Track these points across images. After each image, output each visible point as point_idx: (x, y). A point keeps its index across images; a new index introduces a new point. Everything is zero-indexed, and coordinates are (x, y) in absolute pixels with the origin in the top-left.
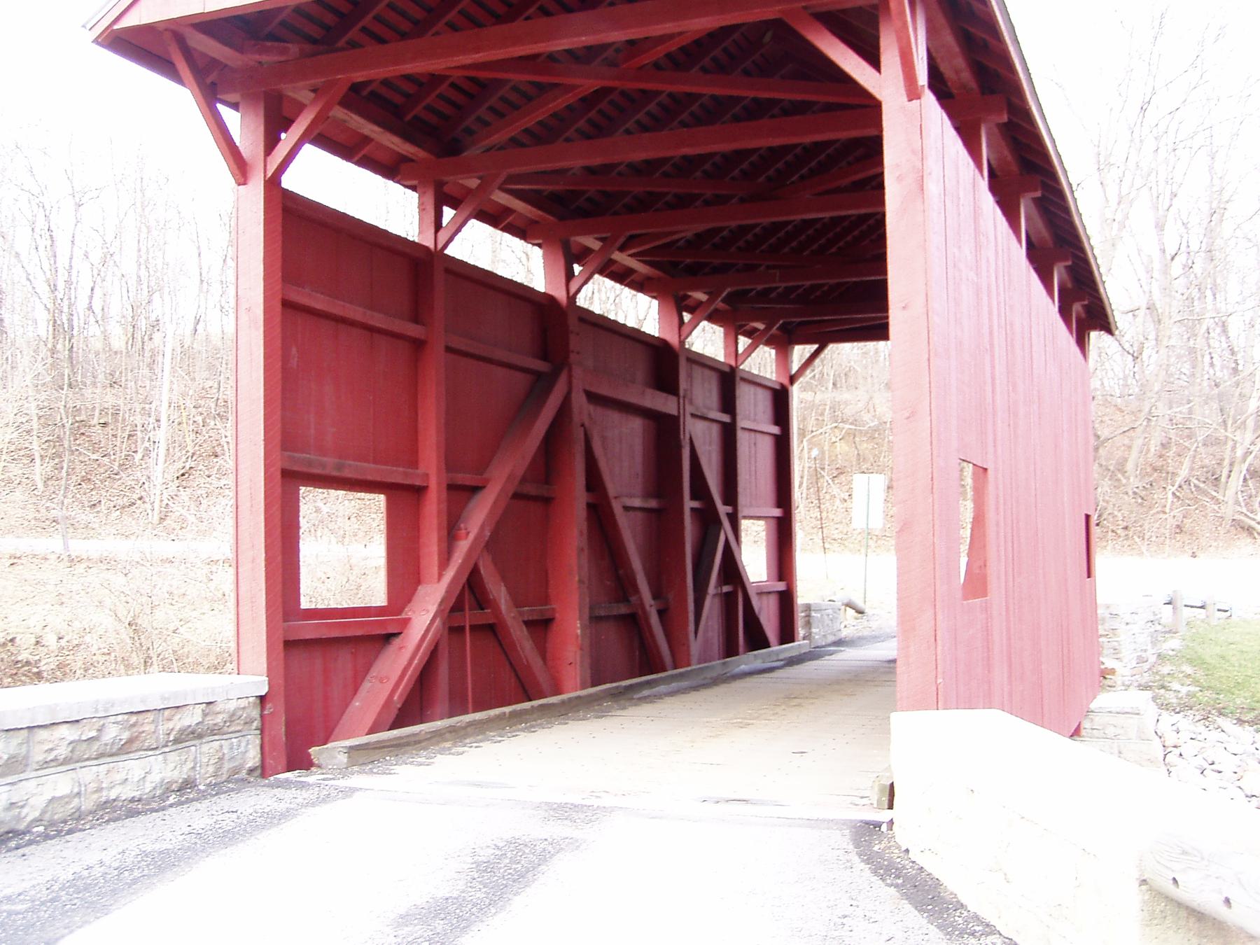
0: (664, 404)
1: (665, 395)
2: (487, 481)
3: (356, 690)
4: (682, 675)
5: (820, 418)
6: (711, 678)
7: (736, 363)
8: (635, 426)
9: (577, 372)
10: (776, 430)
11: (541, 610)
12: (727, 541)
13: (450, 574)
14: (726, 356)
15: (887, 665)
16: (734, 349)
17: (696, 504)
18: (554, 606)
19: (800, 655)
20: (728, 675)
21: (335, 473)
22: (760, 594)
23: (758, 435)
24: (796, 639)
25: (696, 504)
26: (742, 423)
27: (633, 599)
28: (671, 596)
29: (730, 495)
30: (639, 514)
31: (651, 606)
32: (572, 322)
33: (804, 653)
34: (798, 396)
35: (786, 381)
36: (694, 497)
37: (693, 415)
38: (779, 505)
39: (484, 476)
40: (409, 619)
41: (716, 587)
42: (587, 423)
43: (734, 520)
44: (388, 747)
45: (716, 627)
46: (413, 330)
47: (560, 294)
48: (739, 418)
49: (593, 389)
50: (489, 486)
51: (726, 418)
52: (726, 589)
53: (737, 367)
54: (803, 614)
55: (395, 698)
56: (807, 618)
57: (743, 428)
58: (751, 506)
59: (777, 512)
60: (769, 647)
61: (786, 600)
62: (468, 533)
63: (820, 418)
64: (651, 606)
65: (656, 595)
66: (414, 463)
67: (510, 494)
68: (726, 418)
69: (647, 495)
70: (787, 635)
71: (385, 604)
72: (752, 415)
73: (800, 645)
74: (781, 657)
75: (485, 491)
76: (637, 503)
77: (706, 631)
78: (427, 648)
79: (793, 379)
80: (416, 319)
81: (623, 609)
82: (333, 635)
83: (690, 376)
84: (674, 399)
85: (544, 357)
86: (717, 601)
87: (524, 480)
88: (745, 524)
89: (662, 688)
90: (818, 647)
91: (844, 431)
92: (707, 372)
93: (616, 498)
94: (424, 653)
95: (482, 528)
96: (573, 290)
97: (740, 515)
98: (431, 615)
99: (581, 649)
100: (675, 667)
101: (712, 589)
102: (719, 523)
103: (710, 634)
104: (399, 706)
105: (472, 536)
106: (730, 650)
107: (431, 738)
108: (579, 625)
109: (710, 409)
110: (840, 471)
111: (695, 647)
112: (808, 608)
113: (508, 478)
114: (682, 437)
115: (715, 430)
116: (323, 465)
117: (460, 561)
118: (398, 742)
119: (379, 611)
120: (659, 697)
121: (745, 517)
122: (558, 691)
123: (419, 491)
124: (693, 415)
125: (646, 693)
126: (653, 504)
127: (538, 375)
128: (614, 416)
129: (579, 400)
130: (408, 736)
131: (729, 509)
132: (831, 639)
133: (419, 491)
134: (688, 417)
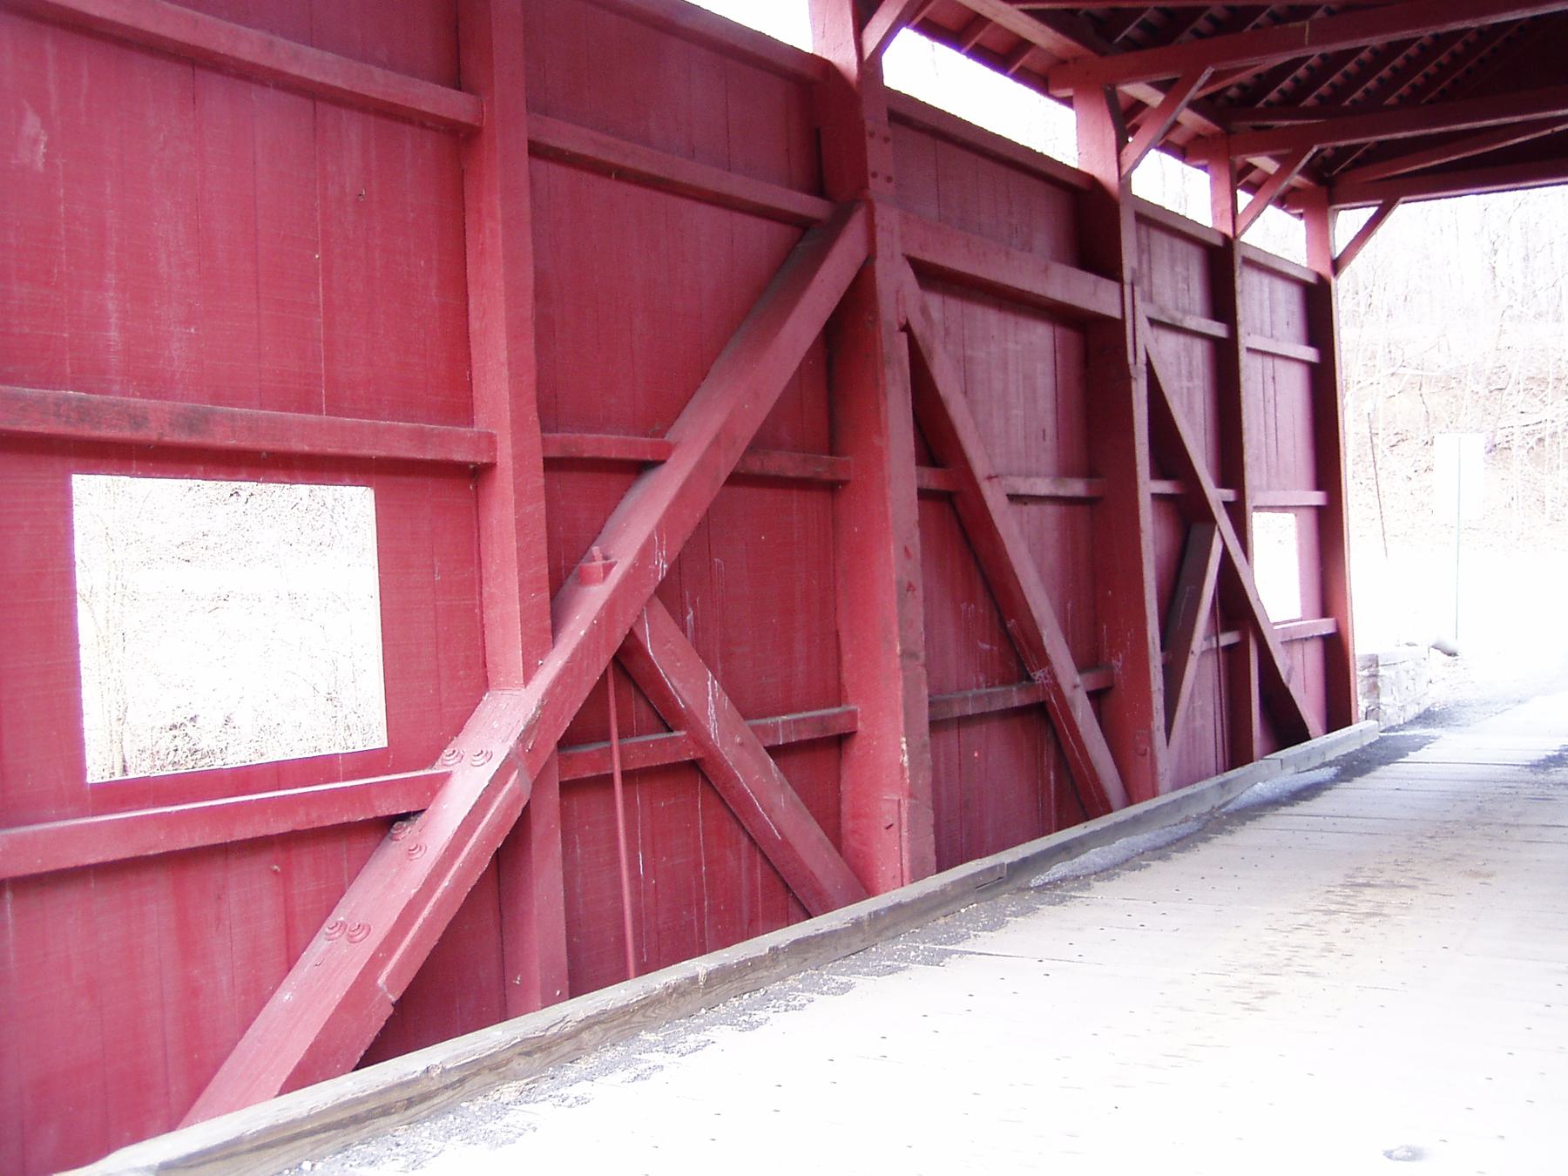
0: (1095, 296)
1: (1092, 277)
2: (669, 449)
3: (290, 962)
4: (1136, 821)
5: (1370, 363)
6: (1199, 818)
7: (1234, 232)
8: (1040, 336)
9: (887, 217)
10: (1310, 354)
11: (822, 718)
12: (1226, 554)
13: (553, 664)
14: (1214, 218)
15: (1533, 777)
16: (1228, 205)
17: (1164, 487)
18: (852, 707)
19: (1363, 750)
20: (1231, 807)
21: (182, 437)
22: (1289, 643)
23: (1279, 363)
24: (1353, 721)
25: (1164, 487)
26: (1246, 340)
27: (1038, 675)
28: (1117, 664)
29: (1231, 468)
30: (1050, 510)
31: (1075, 687)
32: (874, 119)
33: (1371, 745)
34: (1345, 294)
35: (1325, 270)
36: (1158, 473)
37: (1154, 323)
38: (1318, 486)
39: (665, 439)
40: (445, 777)
41: (1207, 638)
42: (917, 329)
43: (1238, 514)
44: (313, 1132)
45: (1210, 709)
46: (451, 104)
47: (845, 58)
48: (1241, 331)
49: (928, 257)
50: (671, 460)
51: (1219, 330)
52: (1227, 639)
53: (1236, 237)
54: (1366, 673)
55: (381, 981)
56: (1371, 680)
57: (1249, 350)
58: (1269, 488)
59: (1317, 498)
60: (1308, 738)
61: (1335, 651)
62: (608, 569)
63: (1370, 363)
64: (1075, 687)
65: (1085, 663)
66: (462, 411)
67: (723, 478)
68: (1219, 330)
69: (1065, 471)
70: (1338, 713)
71: (386, 745)
72: (1267, 328)
73: (1359, 732)
74: (1330, 756)
75: (664, 469)
76: (1043, 487)
77: (1189, 718)
78: (488, 838)
79: (1337, 266)
80: (456, 79)
81: (1016, 697)
82: (184, 843)
83: (1143, 250)
84: (1113, 286)
85: (818, 188)
86: (1210, 665)
87: (760, 443)
88: (1259, 523)
89: (1094, 857)
90: (1391, 729)
91: (1405, 379)
92: (1180, 245)
93: (990, 478)
94: (473, 860)
95: (646, 552)
96: (870, 45)
97: (1249, 505)
98: (495, 765)
99: (911, 796)
100: (1130, 800)
101: (1200, 640)
102: (1211, 520)
103: (1198, 723)
104: (393, 998)
105: (616, 575)
106: (1237, 753)
107: (462, 1081)
108: (904, 746)
109: (1186, 312)
110: (1400, 437)
111: (1166, 758)
112: (1374, 661)
113: (716, 442)
114: (1131, 359)
115: (1199, 350)
116: (137, 420)
117: (582, 633)
118: (353, 1112)
119: (365, 762)
120: (1081, 880)
121: (1258, 508)
122: (864, 888)
123: (476, 475)
124: (1154, 323)
125: (1059, 870)
126: (1077, 488)
127: (802, 225)
128: (988, 319)
129: (895, 281)
130: (381, 1093)
131: (1229, 494)
132: (1413, 711)
133: (476, 475)
134: (1142, 324)
